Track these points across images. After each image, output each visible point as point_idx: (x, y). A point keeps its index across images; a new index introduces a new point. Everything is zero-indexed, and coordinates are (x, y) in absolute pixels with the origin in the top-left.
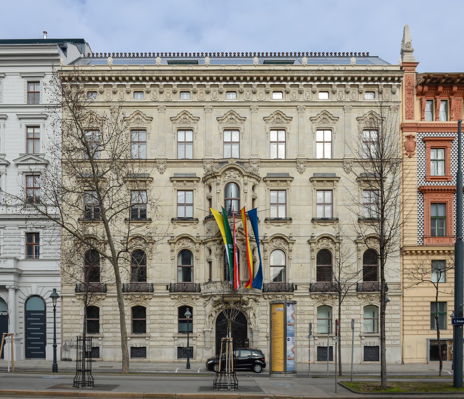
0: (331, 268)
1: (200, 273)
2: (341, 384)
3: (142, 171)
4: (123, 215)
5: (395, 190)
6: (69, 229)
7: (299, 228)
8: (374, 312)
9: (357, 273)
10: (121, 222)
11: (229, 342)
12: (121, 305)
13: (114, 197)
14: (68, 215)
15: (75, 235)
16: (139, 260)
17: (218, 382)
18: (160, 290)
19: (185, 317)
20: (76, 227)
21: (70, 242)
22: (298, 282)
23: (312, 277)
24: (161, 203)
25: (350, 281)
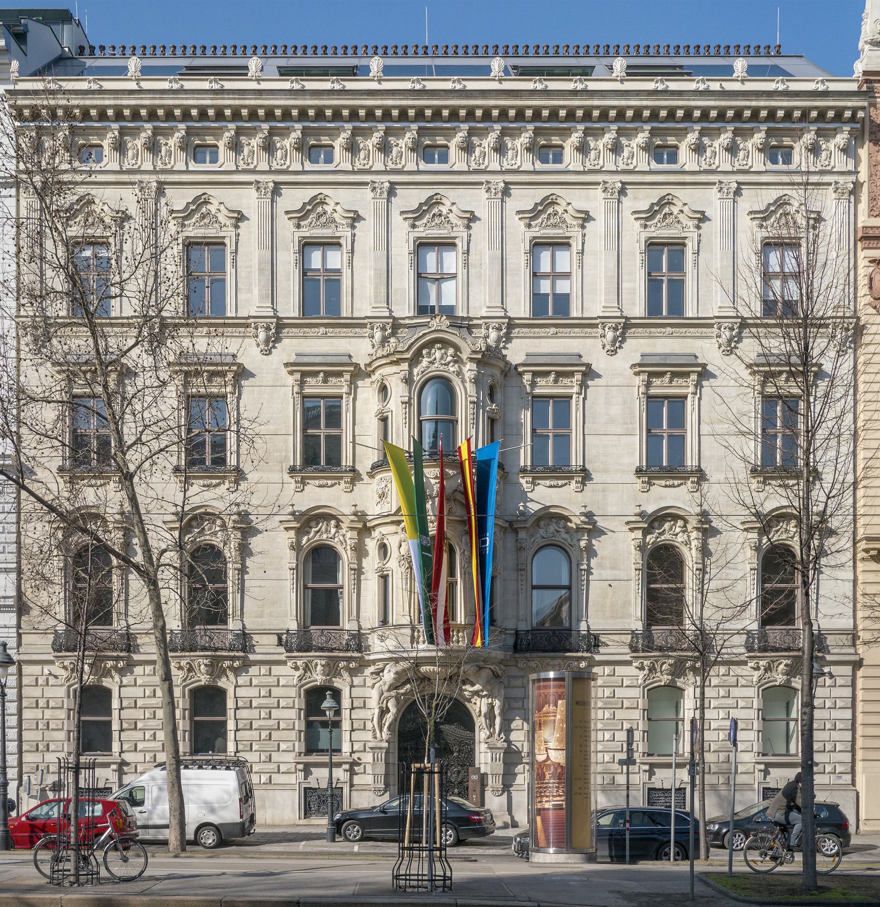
0: (680, 591)
1: (361, 606)
2: (704, 878)
3: (217, 346)
4: (170, 458)
5: (839, 400)
6: (37, 493)
7: (604, 491)
8: (788, 703)
9: (745, 606)
10: (165, 477)
11: (431, 773)
12: (167, 677)
13: (146, 414)
14: (34, 458)
15: (52, 509)
16: (207, 577)
17: (402, 872)
18: (265, 646)
19: (323, 713)
20: (53, 487)
21: (39, 526)
22: (601, 628)
23: (634, 618)
24: (263, 430)
25: (728, 626)
